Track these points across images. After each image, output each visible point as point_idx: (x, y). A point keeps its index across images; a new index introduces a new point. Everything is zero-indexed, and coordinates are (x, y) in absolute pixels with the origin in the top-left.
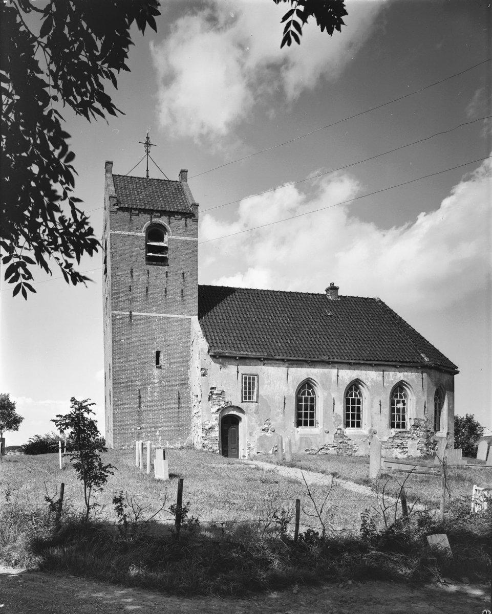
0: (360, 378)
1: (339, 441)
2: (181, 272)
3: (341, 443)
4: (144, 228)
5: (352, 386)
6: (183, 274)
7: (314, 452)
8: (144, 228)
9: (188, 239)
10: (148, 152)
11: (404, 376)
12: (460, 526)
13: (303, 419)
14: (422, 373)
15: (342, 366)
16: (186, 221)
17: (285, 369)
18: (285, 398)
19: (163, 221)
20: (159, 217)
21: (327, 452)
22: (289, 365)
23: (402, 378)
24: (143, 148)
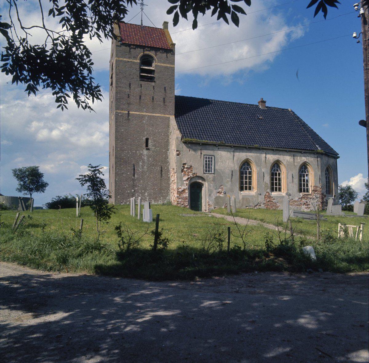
0: (280, 159)
1: (268, 200)
3: (269, 201)
5: (275, 164)
6: (165, 88)
7: (251, 207)
10: (142, 9)
11: (306, 159)
14: (317, 158)
15: (269, 151)
17: (232, 153)
18: (232, 172)
19: (152, 53)
20: (149, 51)
21: (260, 207)
22: (235, 149)
23: (305, 160)
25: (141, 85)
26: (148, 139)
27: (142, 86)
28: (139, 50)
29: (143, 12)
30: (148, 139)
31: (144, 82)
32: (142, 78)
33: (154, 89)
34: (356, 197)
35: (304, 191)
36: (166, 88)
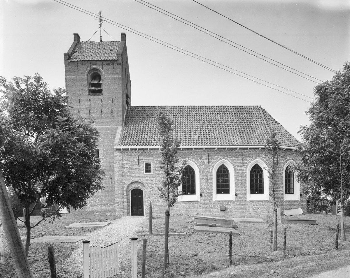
2: (111, 99)
4: (86, 72)
6: (112, 99)
8: (86, 72)
9: (115, 76)
10: (101, 25)
12: (38, 161)
13: (191, 189)
16: (113, 65)
19: (98, 67)
20: (96, 64)
24: (98, 23)
25: (90, 99)
26: (99, 150)
27: (91, 100)
28: (85, 66)
29: (100, 28)
30: (99, 150)
31: (93, 96)
32: (93, 92)
33: (102, 102)
34: (81, 207)
35: (246, 193)
36: (114, 100)
